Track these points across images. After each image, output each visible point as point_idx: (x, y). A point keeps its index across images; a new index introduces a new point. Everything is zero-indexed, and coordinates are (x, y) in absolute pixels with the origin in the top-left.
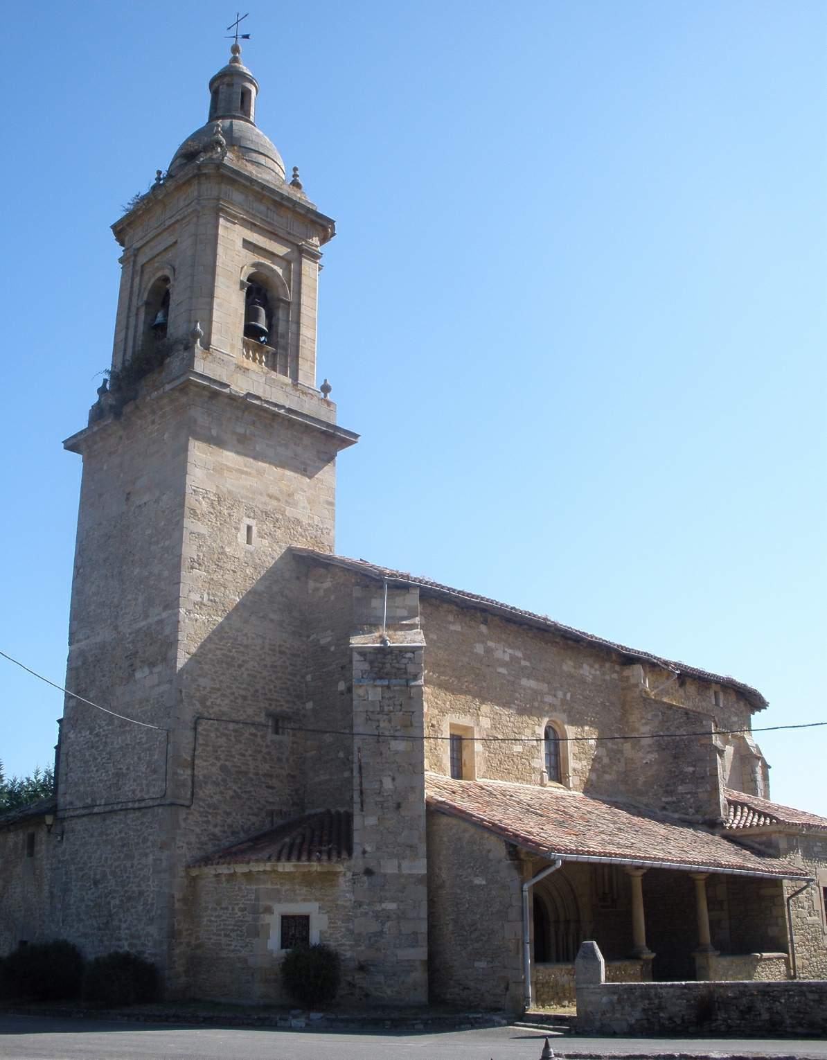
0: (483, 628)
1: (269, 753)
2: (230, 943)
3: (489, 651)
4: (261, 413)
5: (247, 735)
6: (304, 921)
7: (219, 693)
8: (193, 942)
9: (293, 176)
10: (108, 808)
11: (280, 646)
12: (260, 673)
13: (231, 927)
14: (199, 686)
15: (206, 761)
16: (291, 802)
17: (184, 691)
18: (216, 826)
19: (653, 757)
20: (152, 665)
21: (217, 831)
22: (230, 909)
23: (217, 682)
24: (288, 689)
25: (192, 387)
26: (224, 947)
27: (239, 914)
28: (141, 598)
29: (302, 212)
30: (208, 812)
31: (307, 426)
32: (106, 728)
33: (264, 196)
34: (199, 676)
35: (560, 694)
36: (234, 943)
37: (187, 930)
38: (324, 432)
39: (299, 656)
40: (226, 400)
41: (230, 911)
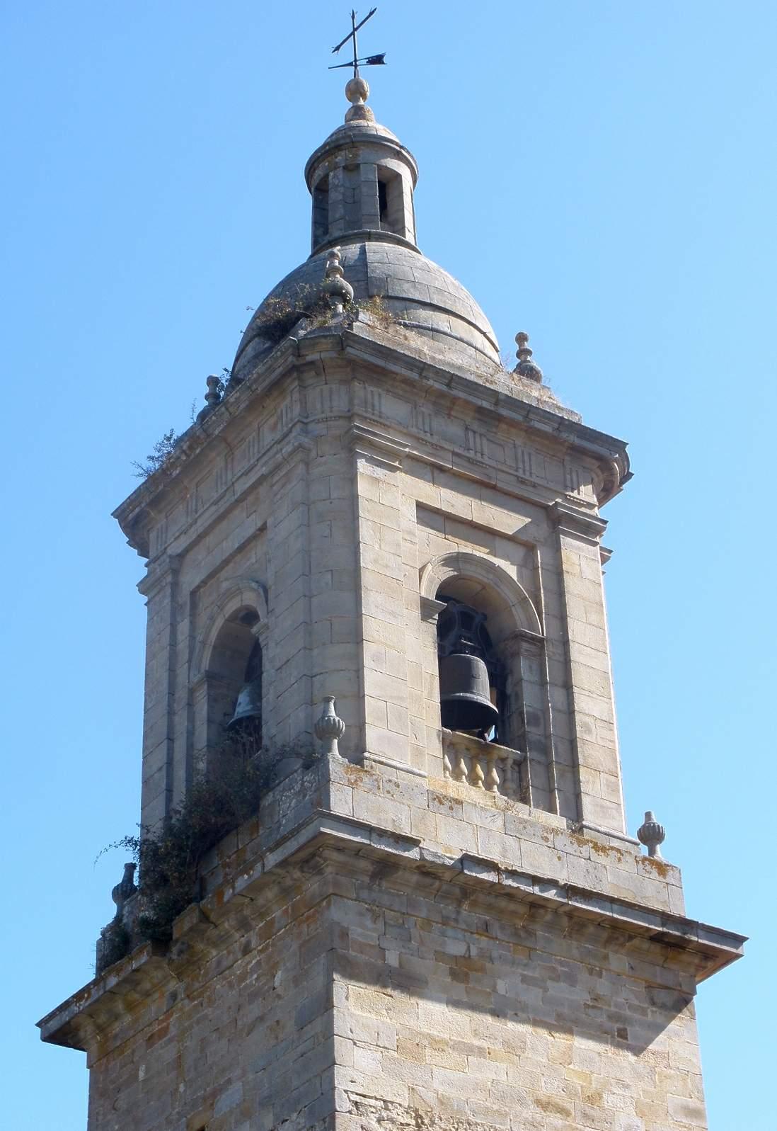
4: (503, 903)
29: (547, 428)
31: (615, 925)
33: (454, 400)
38: (658, 938)
40: (415, 878)
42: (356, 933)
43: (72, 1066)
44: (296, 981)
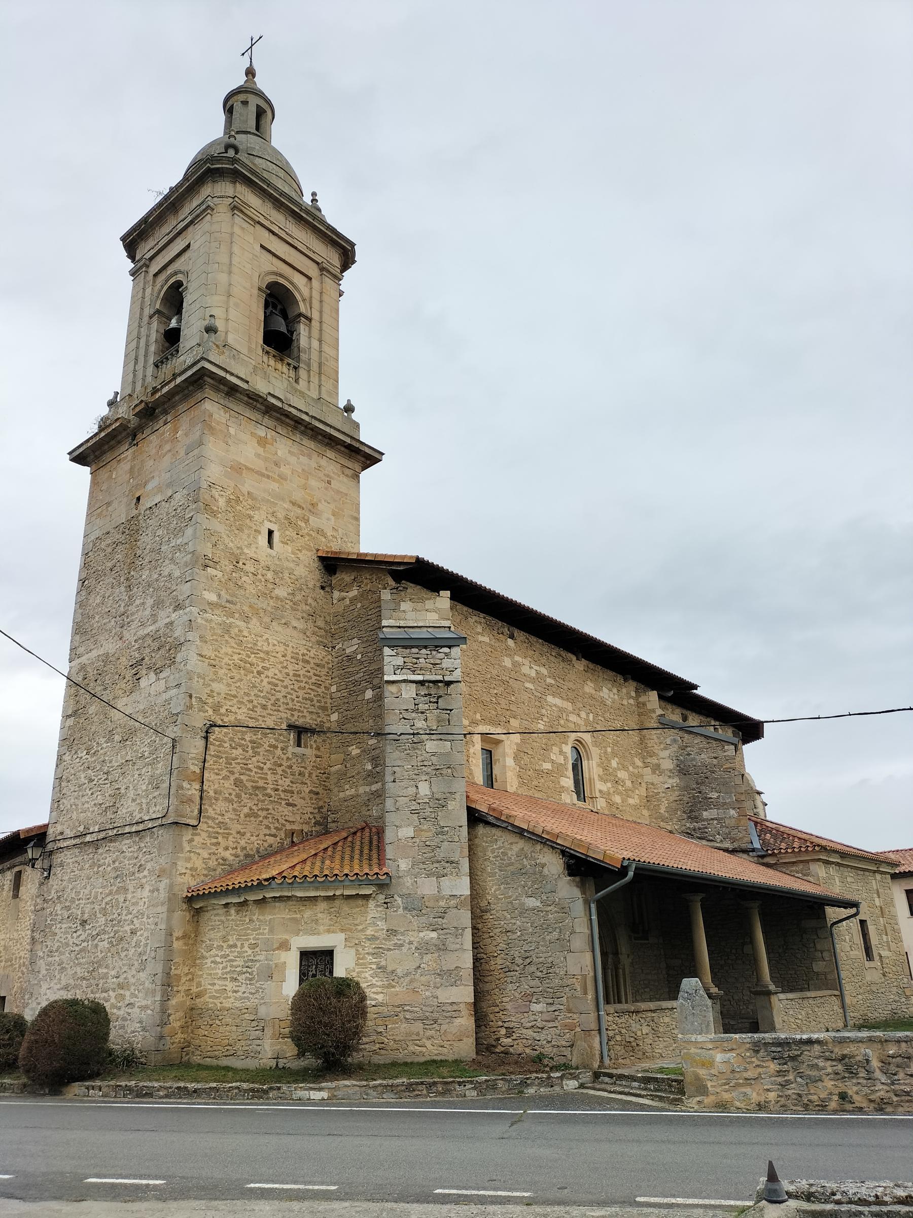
0: (510, 642)
1: (290, 767)
2: (236, 989)
3: (516, 664)
5: (266, 746)
6: (327, 955)
7: (235, 700)
8: (194, 990)
9: (312, 201)
10: (102, 835)
11: (303, 655)
12: (283, 681)
13: (238, 969)
14: (212, 691)
15: (217, 774)
16: (313, 821)
17: (194, 695)
18: (226, 849)
19: (675, 781)
20: (158, 671)
21: (227, 854)
22: (239, 945)
23: (233, 688)
24: (312, 701)
25: (206, 378)
26: (230, 994)
27: (250, 952)
28: (150, 602)
30: (217, 833)
32: (105, 745)
34: (212, 681)
35: (583, 715)
36: (242, 989)
37: (187, 974)
39: (323, 667)
41: (239, 949)
42: (216, 416)
43: (85, 472)
44: (186, 435)
